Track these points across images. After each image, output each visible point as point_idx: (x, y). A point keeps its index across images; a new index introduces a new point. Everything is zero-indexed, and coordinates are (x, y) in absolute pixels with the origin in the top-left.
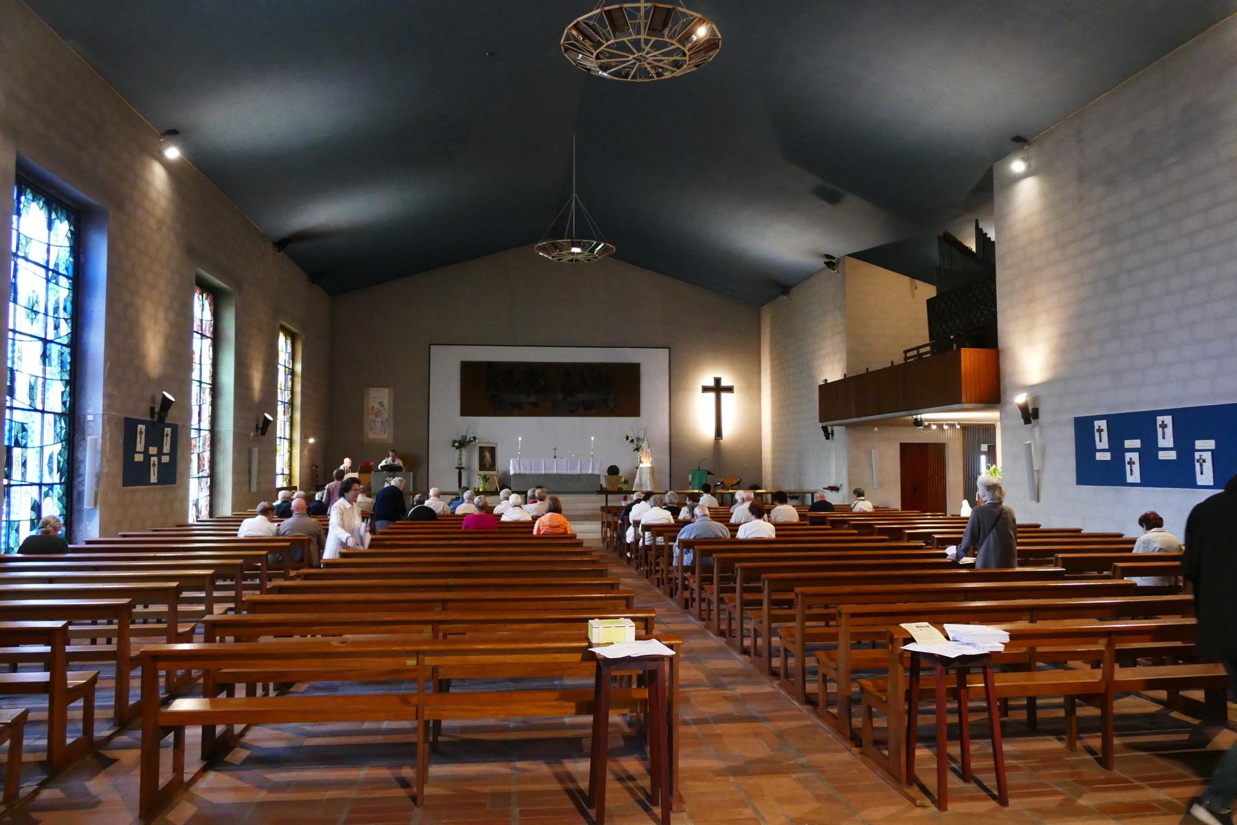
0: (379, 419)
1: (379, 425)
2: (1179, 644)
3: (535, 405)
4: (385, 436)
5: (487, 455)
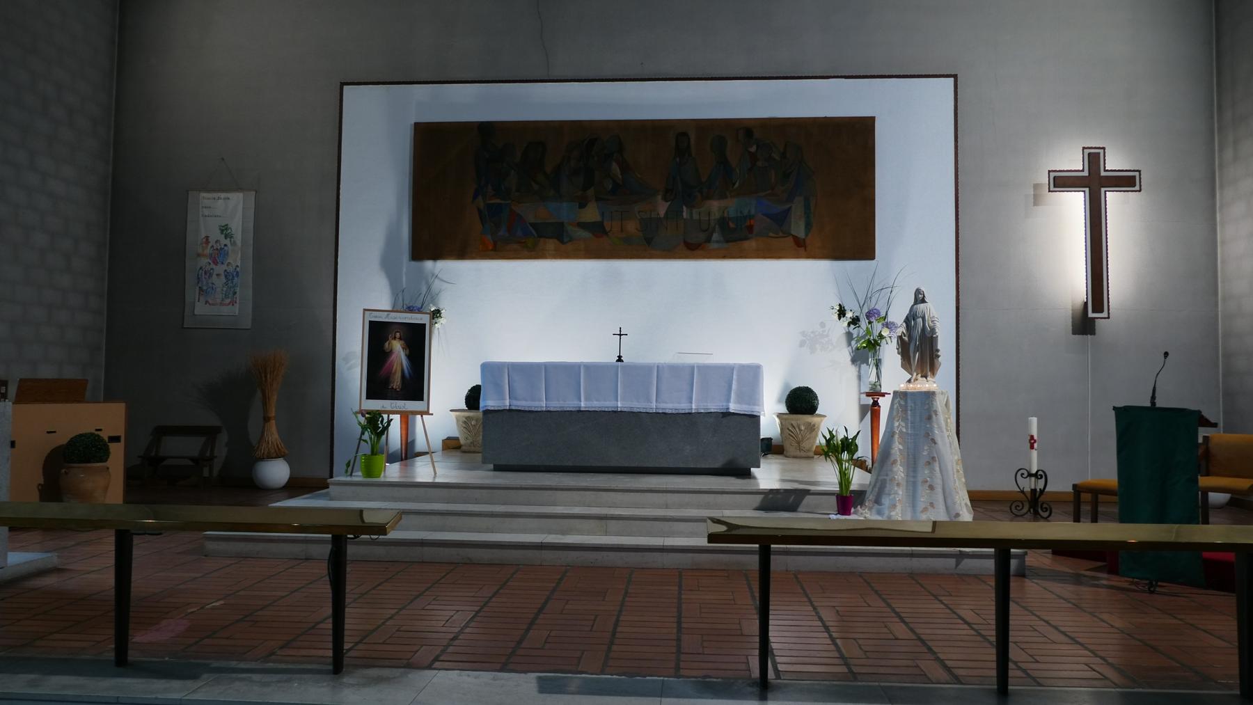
0: (220, 269)
1: (219, 282)
2: (498, 201)
3: (598, 229)
4: (235, 310)
5: (398, 349)
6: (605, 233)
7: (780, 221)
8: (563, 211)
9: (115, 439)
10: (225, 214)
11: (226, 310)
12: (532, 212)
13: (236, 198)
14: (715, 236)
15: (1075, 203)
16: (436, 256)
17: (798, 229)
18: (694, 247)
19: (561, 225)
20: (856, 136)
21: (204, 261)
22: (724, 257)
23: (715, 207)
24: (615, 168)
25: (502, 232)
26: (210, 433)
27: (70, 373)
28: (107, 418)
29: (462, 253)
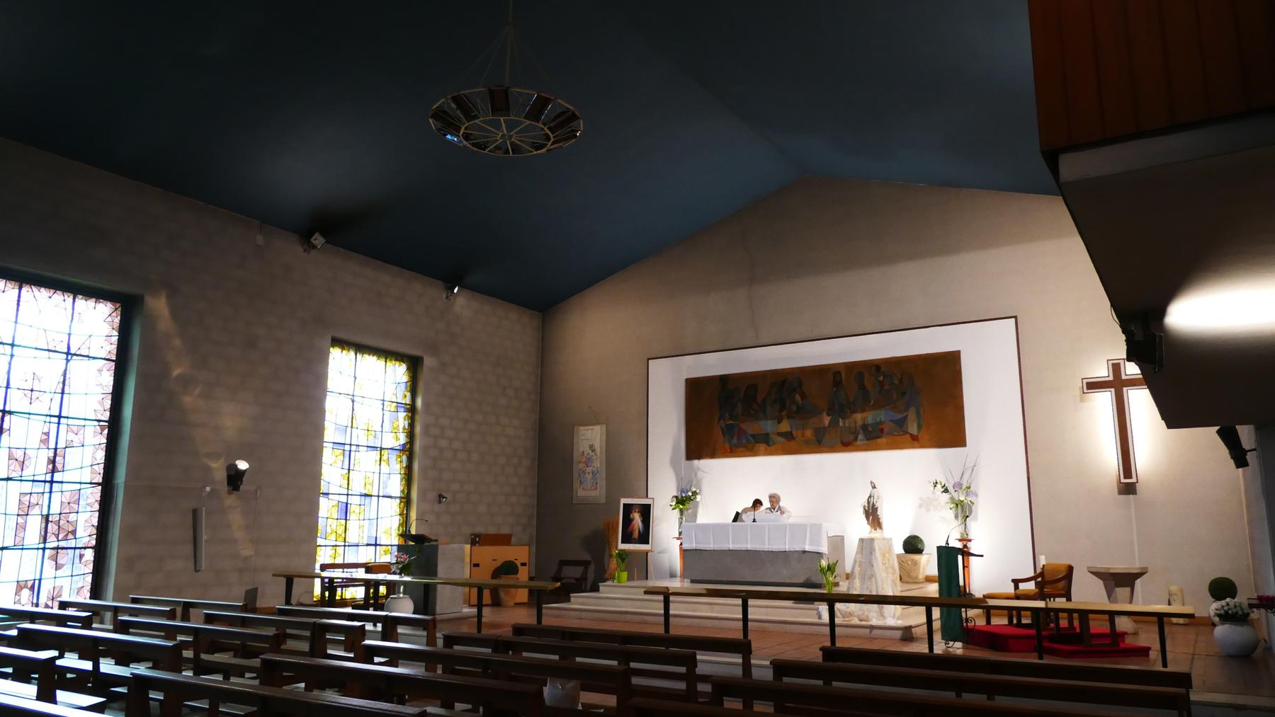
0: (589, 469)
1: (589, 477)
3: (789, 436)
5: (637, 518)
6: (794, 439)
7: (901, 424)
8: (768, 426)
9: (523, 564)
10: (591, 438)
11: (593, 493)
12: (751, 428)
13: (597, 428)
14: (860, 437)
15: (1104, 400)
16: (699, 458)
17: (913, 429)
18: (847, 444)
19: (768, 434)
20: (948, 365)
21: (581, 466)
22: (866, 450)
23: (858, 417)
24: (798, 397)
25: (735, 441)
26: (585, 564)
27: (505, 530)
28: (519, 554)
29: (713, 455)
